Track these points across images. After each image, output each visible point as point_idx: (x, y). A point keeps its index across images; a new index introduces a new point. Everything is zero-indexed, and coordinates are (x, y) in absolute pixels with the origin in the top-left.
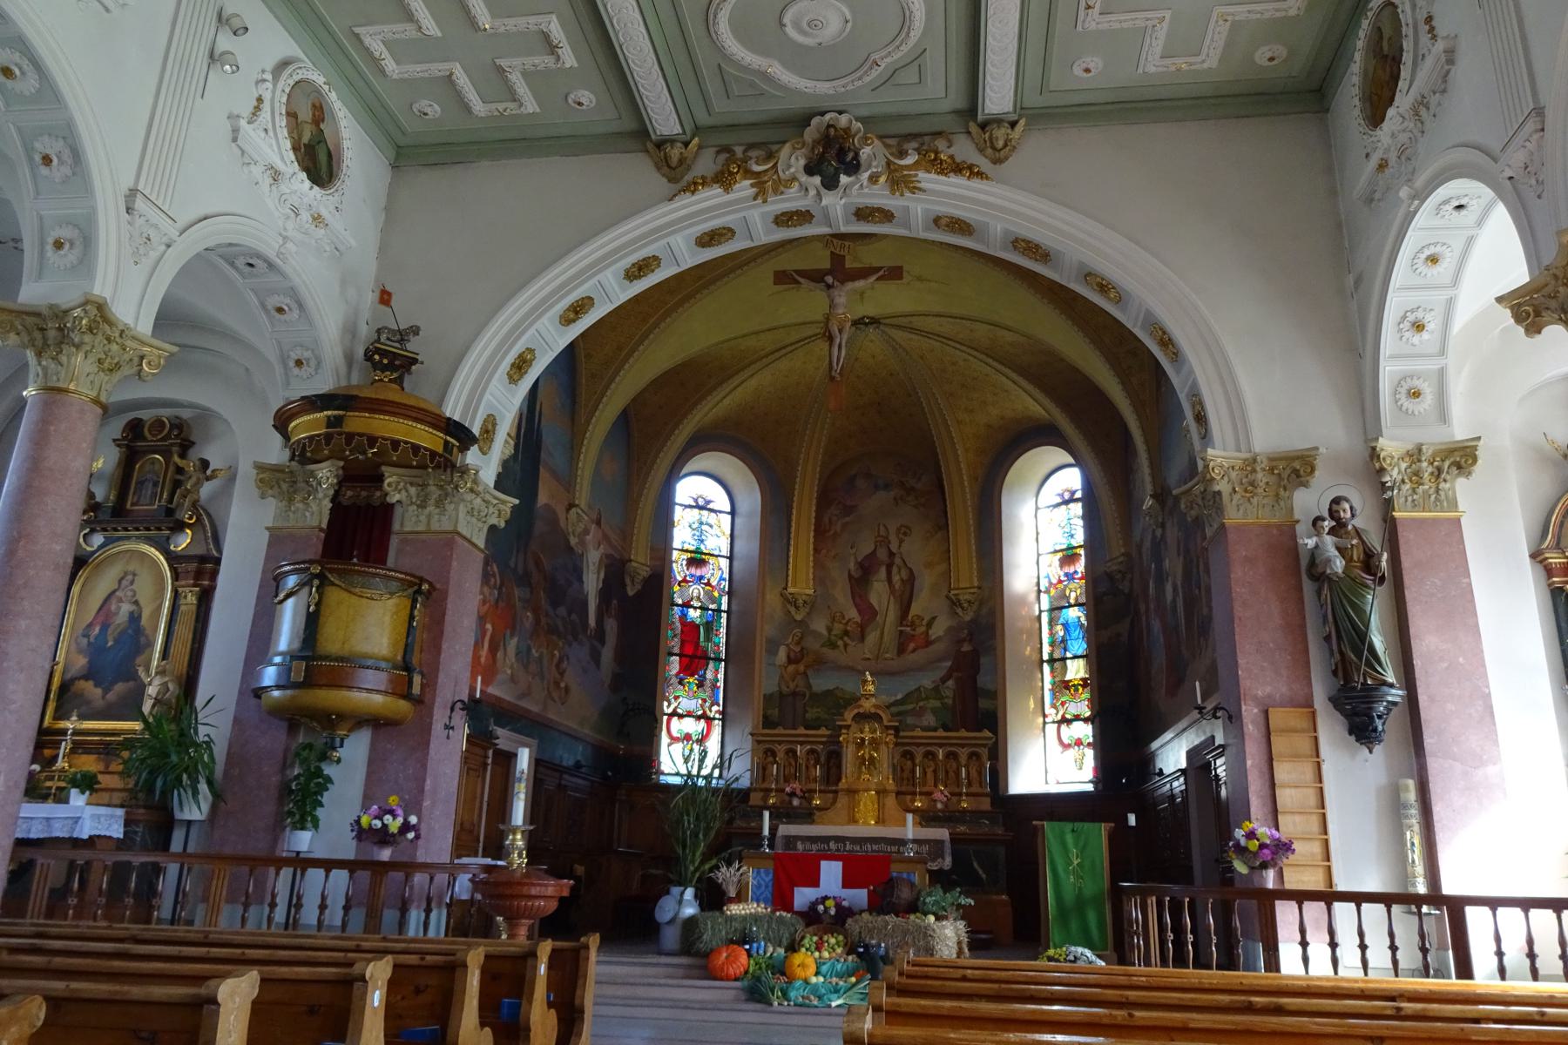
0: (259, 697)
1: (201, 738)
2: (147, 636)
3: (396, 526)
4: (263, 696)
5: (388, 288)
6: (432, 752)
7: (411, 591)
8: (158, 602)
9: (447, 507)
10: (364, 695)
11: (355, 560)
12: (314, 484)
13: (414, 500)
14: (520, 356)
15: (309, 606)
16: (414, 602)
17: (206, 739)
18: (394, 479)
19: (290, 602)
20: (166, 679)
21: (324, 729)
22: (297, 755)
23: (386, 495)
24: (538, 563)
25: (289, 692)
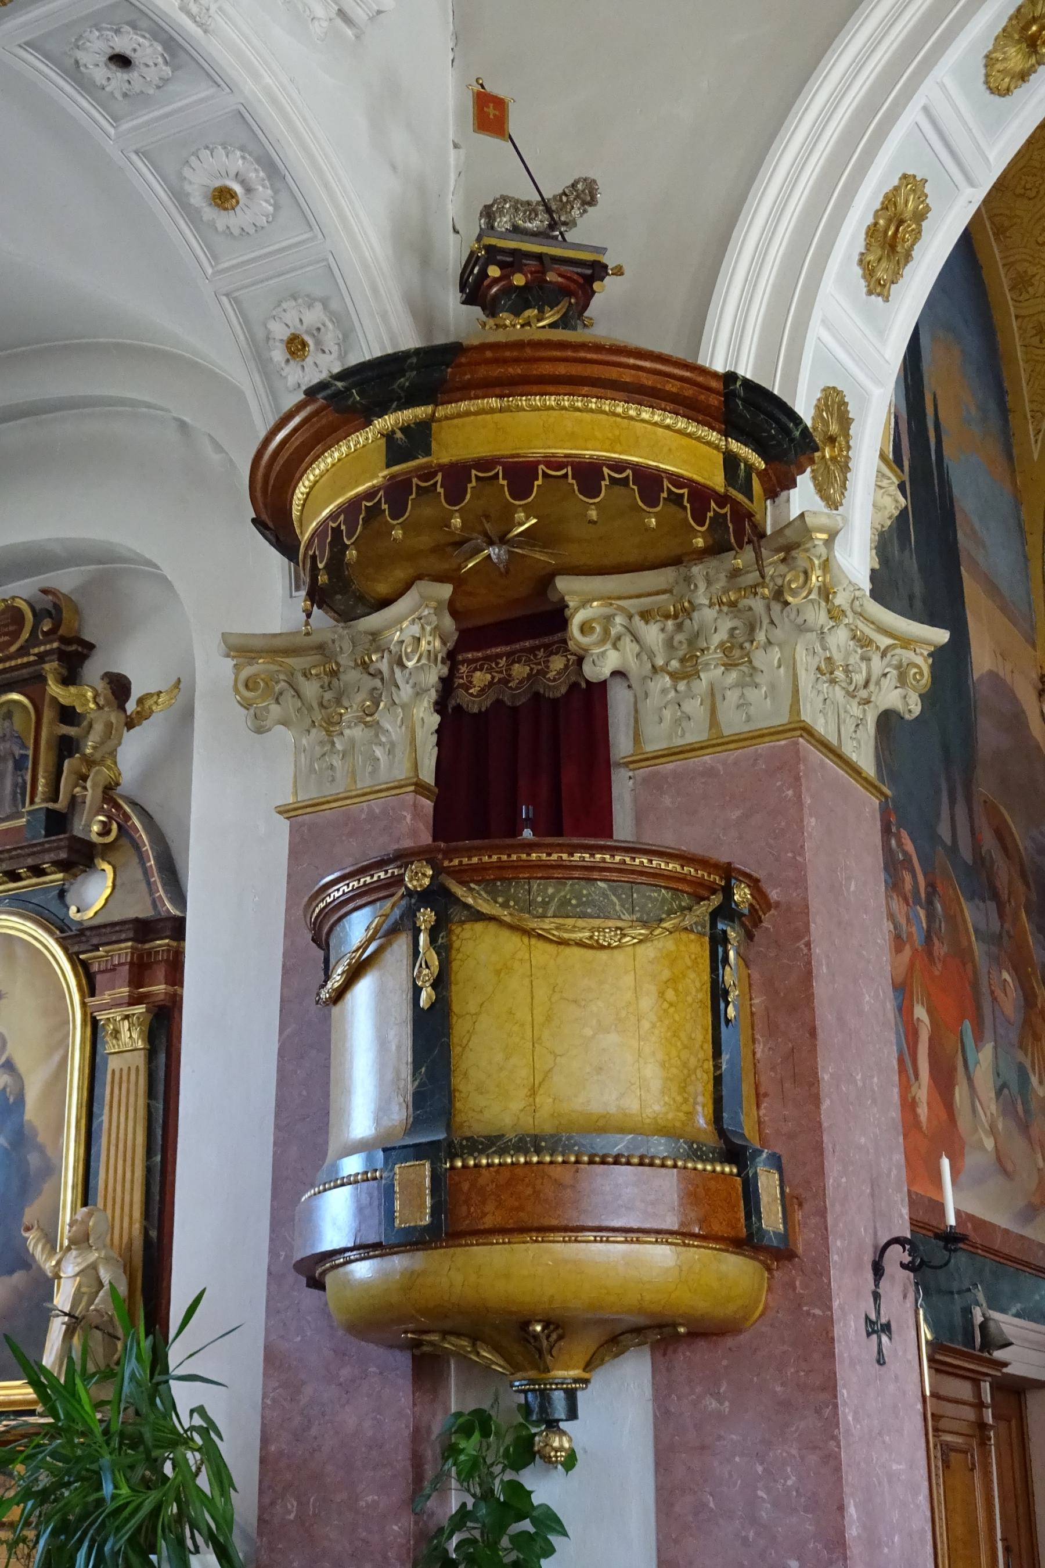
0: (317, 1284)
1: (185, 1419)
2: (41, 1149)
3: (621, 744)
4: (329, 1280)
5: (494, 88)
6: (847, 1414)
7: (703, 910)
8: (57, 1058)
9: (760, 658)
10: (616, 1250)
11: (527, 833)
12: (384, 666)
13: (660, 662)
14: (889, 202)
15: (417, 991)
16: (718, 941)
17: (197, 1421)
18: (596, 607)
19: (364, 990)
20: (94, 1256)
21: (516, 1367)
22: (451, 1451)
23: (580, 660)
24: (1001, 834)
25: (398, 1263)
